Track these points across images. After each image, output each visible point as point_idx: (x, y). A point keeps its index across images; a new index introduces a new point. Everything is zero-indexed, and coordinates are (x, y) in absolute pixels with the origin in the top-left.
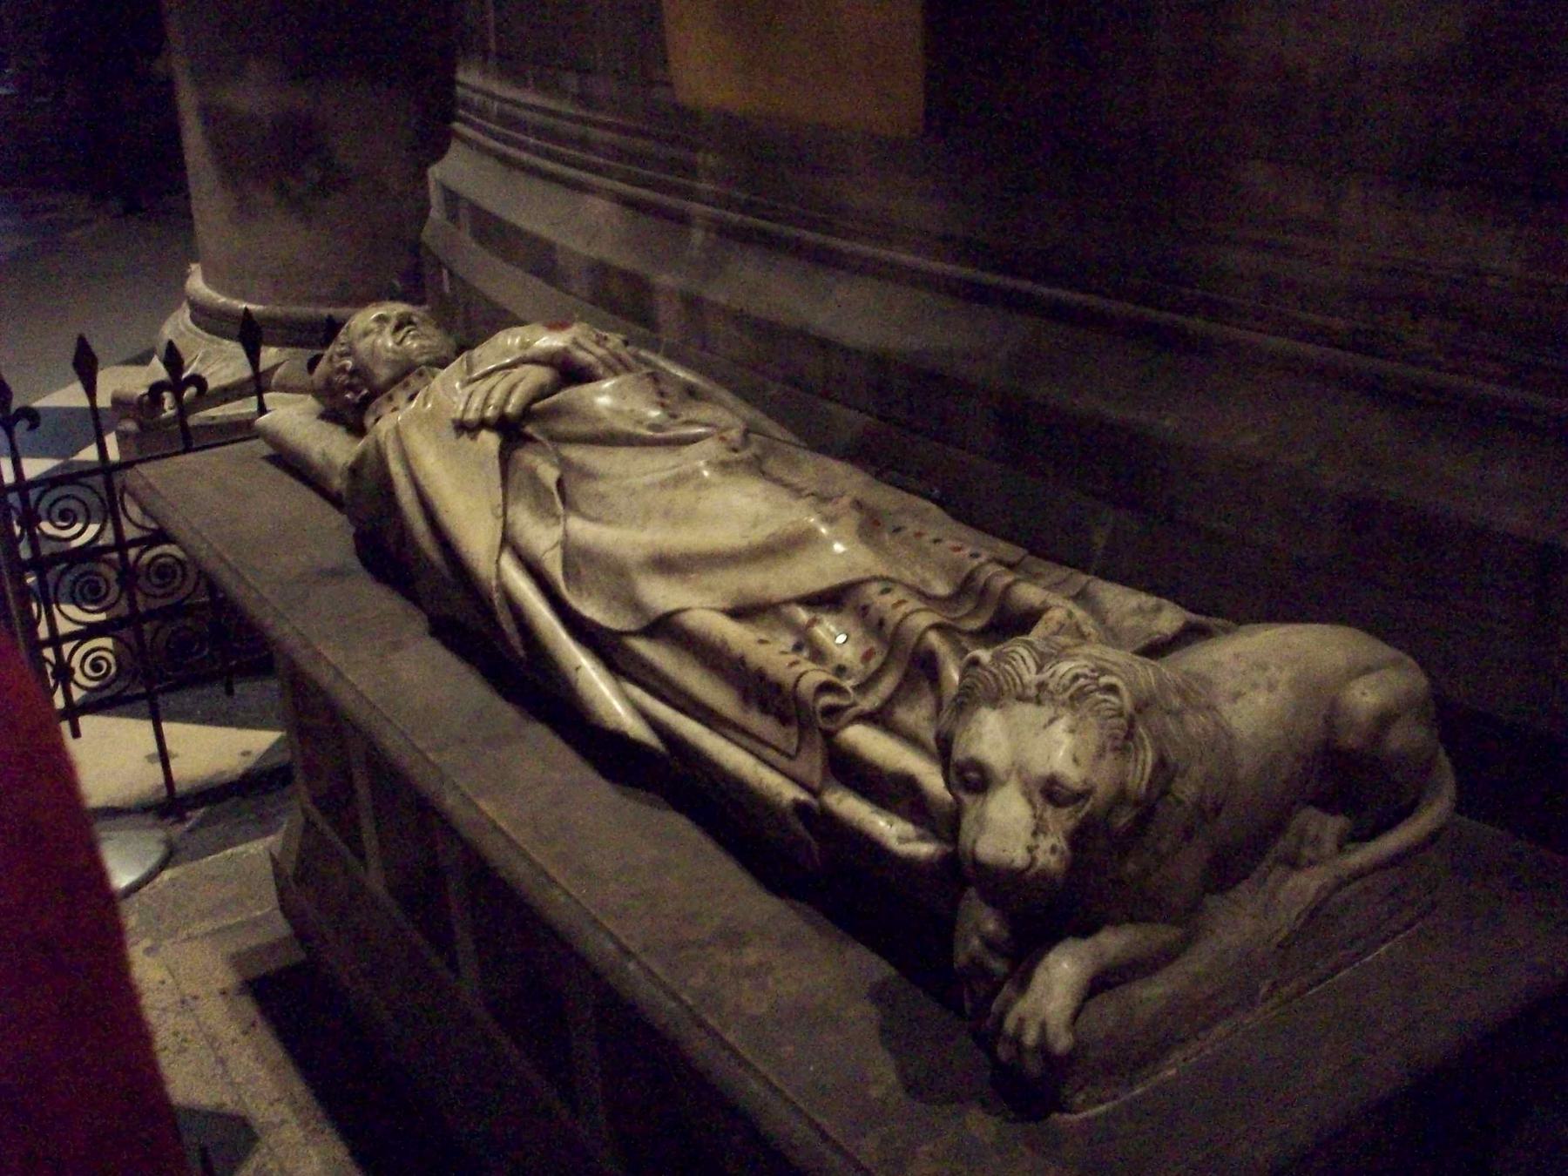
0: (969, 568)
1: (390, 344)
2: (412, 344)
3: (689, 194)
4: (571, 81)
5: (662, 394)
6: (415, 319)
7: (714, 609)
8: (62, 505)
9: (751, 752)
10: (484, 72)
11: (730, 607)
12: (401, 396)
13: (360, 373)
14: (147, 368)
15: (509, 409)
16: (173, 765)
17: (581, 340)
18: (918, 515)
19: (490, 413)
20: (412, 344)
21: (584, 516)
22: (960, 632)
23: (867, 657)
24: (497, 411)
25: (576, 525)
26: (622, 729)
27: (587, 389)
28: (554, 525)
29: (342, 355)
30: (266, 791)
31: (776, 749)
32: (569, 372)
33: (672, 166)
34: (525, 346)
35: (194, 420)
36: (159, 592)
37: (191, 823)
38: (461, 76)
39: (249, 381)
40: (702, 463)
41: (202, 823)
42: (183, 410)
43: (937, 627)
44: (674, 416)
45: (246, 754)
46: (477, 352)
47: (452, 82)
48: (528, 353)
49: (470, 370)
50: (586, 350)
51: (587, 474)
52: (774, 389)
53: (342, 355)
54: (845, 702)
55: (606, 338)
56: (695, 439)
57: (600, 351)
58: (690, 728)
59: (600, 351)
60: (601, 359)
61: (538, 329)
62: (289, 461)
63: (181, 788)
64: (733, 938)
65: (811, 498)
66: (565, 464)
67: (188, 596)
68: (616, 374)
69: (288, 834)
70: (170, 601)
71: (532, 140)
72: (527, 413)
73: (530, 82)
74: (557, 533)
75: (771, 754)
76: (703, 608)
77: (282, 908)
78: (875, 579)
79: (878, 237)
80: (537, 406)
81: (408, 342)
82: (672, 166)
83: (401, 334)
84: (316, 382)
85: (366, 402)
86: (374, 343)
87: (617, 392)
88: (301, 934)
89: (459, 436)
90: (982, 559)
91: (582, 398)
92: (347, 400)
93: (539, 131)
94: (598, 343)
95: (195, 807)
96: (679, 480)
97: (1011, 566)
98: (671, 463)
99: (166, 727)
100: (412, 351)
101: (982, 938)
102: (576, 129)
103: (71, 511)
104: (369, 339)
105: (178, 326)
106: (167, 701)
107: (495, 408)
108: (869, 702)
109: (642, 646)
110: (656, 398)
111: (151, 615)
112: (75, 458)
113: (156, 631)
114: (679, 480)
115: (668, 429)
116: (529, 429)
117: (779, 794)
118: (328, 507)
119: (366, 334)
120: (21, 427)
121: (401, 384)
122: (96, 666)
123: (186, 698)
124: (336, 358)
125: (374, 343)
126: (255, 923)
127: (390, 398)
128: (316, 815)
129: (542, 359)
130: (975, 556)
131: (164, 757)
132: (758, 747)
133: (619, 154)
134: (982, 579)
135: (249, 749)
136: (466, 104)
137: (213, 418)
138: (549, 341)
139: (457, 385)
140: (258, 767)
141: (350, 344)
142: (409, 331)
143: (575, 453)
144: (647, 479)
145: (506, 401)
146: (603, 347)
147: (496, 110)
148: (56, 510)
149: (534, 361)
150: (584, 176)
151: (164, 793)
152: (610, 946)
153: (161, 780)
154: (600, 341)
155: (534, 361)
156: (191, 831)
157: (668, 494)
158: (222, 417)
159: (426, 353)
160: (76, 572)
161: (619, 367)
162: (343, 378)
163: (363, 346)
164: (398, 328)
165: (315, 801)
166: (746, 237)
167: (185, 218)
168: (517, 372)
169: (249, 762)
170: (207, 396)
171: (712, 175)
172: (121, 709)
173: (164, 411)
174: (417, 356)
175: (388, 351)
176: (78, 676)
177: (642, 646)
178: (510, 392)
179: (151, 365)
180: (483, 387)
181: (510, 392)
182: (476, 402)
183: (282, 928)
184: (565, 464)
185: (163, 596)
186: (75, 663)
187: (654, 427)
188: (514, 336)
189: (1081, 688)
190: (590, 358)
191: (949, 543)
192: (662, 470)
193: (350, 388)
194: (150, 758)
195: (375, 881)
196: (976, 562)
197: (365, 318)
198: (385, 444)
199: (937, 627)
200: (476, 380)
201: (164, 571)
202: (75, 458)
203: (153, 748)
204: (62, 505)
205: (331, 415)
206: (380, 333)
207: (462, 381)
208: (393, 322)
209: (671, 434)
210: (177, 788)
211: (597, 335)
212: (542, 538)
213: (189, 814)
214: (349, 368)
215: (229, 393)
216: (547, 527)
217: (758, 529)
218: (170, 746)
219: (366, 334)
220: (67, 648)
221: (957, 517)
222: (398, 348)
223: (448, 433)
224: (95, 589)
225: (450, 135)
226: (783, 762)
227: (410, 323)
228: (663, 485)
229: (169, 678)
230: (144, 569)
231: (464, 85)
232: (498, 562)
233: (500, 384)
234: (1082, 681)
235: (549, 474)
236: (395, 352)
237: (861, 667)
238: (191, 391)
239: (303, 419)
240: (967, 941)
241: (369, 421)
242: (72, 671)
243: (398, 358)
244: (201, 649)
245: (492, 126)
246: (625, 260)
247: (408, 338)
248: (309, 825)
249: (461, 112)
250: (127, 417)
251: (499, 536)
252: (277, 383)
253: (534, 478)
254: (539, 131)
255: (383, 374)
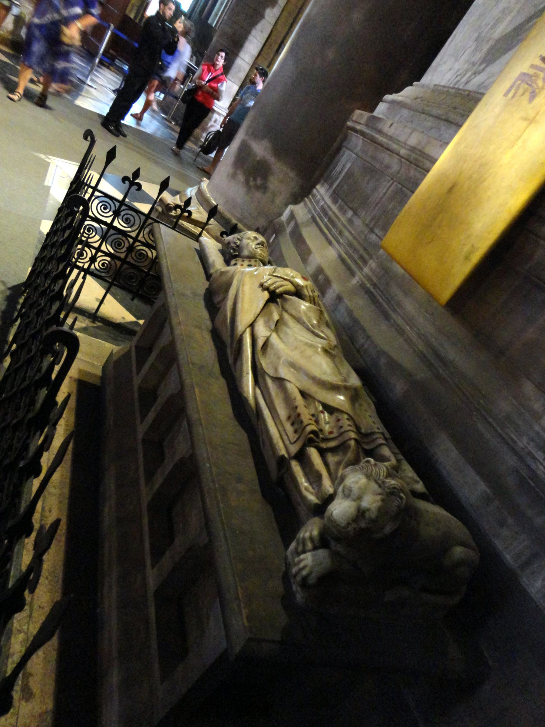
0: (374, 431)
1: (253, 247)
2: (259, 251)
3: (361, 269)
4: (350, 213)
5: (320, 318)
6: (264, 245)
7: (297, 387)
8: (128, 216)
9: (280, 433)
10: (327, 191)
11: (302, 389)
12: (246, 263)
13: (239, 248)
14: (173, 198)
15: (277, 291)
16: (102, 306)
17: (308, 287)
18: (369, 404)
19: (272, 288)
20: (259, 251)
21: (278, 335)
22: (361, 446)
23: (331, 433)
24: (274, 289)
25: (274, 336)
26: (248, 399)
27: (301, 301)
28: (269, 331)
29: (238, 239)
30: (121, 332)
31: (288, 437)
32: (298, 293)
33: (362, 258)
34: (293, 277)
35: (181, 222)
36: (135, 258)
37: (95, 325)
38: (318, 187)
39: (204, 223)
40: (320, 346)
41: (98, 327)
42: (180, 217)
43: (355, 439)
44: (319, 327)
45: (124, 318)
46: (279, 268)
47: (314, 186)
48: (292, 279)
49: (274, 272)
50: (308, 291)
51: (285, 324)
52: (345, 337)
53: (238, 239)
54: (317, 440)
55: (315, 291)
56: (322, 338)
57: (311, 294)
58: (266, 413)
59: (311, 294)
60: (310, 296)
61: (299, 276)
62: (202, 255)
63: (99, 313)
64: (239, 480)
65: (343, 378)
66: (281, 316)
67: (142, 267)
68: (311, 303)
69: (121, 350)
70: (136, 264)
71: (326, 220)
72: (281, 295)
73: (338, 205)
74: (268, 334)
75: (285, 438)
76: (295, 385)
77: (103, 367)
78: (347, 414)
79: (131, 149)
80: (285, 295)
81: (258, 250)
82: (362, 258)
83: (258, 246)
84: (225, 240)
85: (236, 257)
86: (248, 244)
87: (308, 308)
88: (103, 378)
89: (259, 287)
90: (379, 431)
91: (299, 303)
92: (231, 252)
93: (330, 219)
94: (312, 291)
95: (99, 322)
96: (311, 346)
97: (386, 439)
98: (311, 339)
99: (109, 296)
100: (258, 253)
101: (311, 534)
102: (341, 227)
103: (130, 219)
104: (249, 241)
105: (191, 192)
106: (113, 289)
107: (274, 288)
108: (324, 445)
109: (269, 382)
110: (318, 318)
111: (129, 263)
112: (133, 203)
113: (126, 269)
114: (311, 346)
115: (315, 329)
116: (278, 300)
117: (280, 450)
118: (204, 276)
119: (249, 239)
120: (135, 187)
121: (249, 259)
122: (103, 265)
123: (119, 291)
124: (236, 239)
125: (248, 244)
126: (93, 365)
127: (243, 261)
128: (133, 349)
129: (294, 283)
130: (378, 428)
131: (101, 302)
132: (283, 433)
133: (350, 245)
134: (375, 436)
135: (125, 318)
136: (314, 196)
137: (183, 225)
138: (300, 281)
139: (268, 273)
140: (126, 324)
141: (242, 238)
142: (261, 247)
143: (286, 316)
144: (302, 338)
145: (278, 288)
146: (313, 293)
147: (321, 204)
148: (125, 217)
149: (292, 283)
150: (333, 240)
151: (94, 311)
152: (205, 455)
153: (96, 306)
154: (313, 291)
155: (292, 283)
156: (93, 327)
157: (306, 347)
158: (186, 226)
159: (262, 257)
160: (117, 236)
161: (313, 302)
162: (234, 245)
163: (245, 241)
164: (258, 244)
165: (136, 347)
166: (368, 292)
167: (366, 266)
168: (278, 279)
169: (122, 321)
170: (189, 219)
171: (371, 270)
172: (100, 280)
173: (172, 213)
174: (258, 255)
175: (252, 247)
176: (96, 264)
177: (269, 382)
178: (281, 286)
179: (175, 197)
180: (274, 279)
181: (281, 286)
182: (270, 282)
183: (99, 372)
184: (281, 316)
185: (135, 261)
186: (99, 260)
187: (312, 325)
188: (292, 272)
189: (394, 492)
190: (307, 293)
191: (374, 420)
192: (308, 339)
193: (233, 249)
194: (97, 299)
195: (137, 381)
196: (377, 431)
197: (252, 234)
198: (237, 273)
199: (355, 439)
200: (274, 276)
201: (142, 256)
202: (133, 203)
203: (101, 298)
204: (128, 216)
205: (223, 252)
206: (253, 241)
207: (270, 273)
208: (258, 242)
209: (316, 331)
210: (98, 313)
211: (313, 289)
212: (262, 331)
213: (96, 322)
214: (237, 244)
215: (196, 223)
216: (266, 330)
217: (325, 376)
218: (105, 301)
219: (249, 239)
220: (100, 254)
221: (378, 414)
222: (255, 249)
223: (257, 284)
224: (120, 245)
225: (302, 200)
226: (287, 442)
227: (263, 245)
228: (306, 344)
229: (120, 283)
230: (136, 250)
231: (317, 190)
232: (246, 329)
233: (280, 282)
234: (396, 490)
235: (276, 317)
236: (253, 250)
237: (327, 434)
238: (186, 214)
239: (214, 247)
240: (306, 531)
241: (233, 262)
242: (96, 261)
243: (253, 252)
244: (134, 282)
245: (317, 208)
246: (329, 272)
247: (260, 249)
248: (129, 352)
249: (310, 197)
250: (161, 206)
251: (251, 322)
252: (207, 229)
253: (271, 314)
254: (330, 219)
255: (246, 253)
